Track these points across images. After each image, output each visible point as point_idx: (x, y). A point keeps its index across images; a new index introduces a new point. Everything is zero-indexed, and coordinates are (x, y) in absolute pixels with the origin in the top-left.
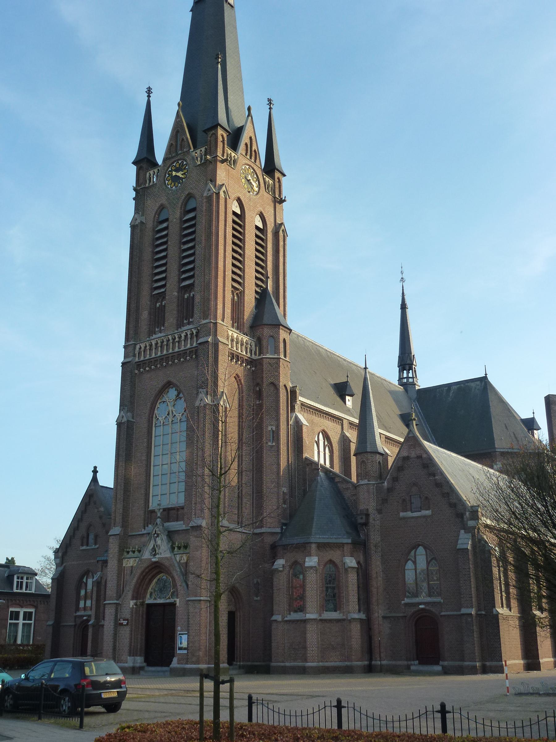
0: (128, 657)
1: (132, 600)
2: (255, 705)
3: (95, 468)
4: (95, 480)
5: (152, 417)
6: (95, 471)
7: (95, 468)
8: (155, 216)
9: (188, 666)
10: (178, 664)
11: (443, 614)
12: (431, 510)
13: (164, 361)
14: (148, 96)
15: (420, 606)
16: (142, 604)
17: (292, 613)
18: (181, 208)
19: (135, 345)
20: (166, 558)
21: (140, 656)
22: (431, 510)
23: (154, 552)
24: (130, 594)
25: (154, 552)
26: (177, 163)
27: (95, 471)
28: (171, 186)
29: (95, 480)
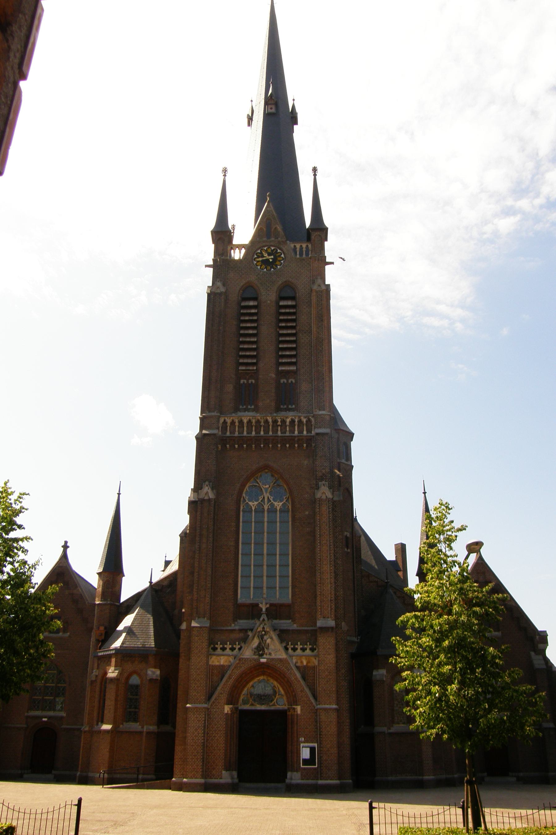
0: (224, 772)
1: (228, 704)
2: (525, 819)
3: (66, 542)
4: (64, 556)
5: (240, 501)
6: (66, 547)
7: (66, 542)
8: (239, 291)
9: (320, 782)
10: (302, 779)
11: (64, 726)
12: (500, 632)
13: (262, 442)
14: (314, 175)
15: (44, 719)
16: (237, 708)
17: (124, 723)
18: (276, 292)
19: (219, 417)
20: (281, 660)
21: (235, 770)
22: (500, 632)
23: (260, 650)
24: (224, 697)
25: (260, 650)
26: (268, 248)
27: (66, 547)
28: (262, 268)
29: (64, 556)
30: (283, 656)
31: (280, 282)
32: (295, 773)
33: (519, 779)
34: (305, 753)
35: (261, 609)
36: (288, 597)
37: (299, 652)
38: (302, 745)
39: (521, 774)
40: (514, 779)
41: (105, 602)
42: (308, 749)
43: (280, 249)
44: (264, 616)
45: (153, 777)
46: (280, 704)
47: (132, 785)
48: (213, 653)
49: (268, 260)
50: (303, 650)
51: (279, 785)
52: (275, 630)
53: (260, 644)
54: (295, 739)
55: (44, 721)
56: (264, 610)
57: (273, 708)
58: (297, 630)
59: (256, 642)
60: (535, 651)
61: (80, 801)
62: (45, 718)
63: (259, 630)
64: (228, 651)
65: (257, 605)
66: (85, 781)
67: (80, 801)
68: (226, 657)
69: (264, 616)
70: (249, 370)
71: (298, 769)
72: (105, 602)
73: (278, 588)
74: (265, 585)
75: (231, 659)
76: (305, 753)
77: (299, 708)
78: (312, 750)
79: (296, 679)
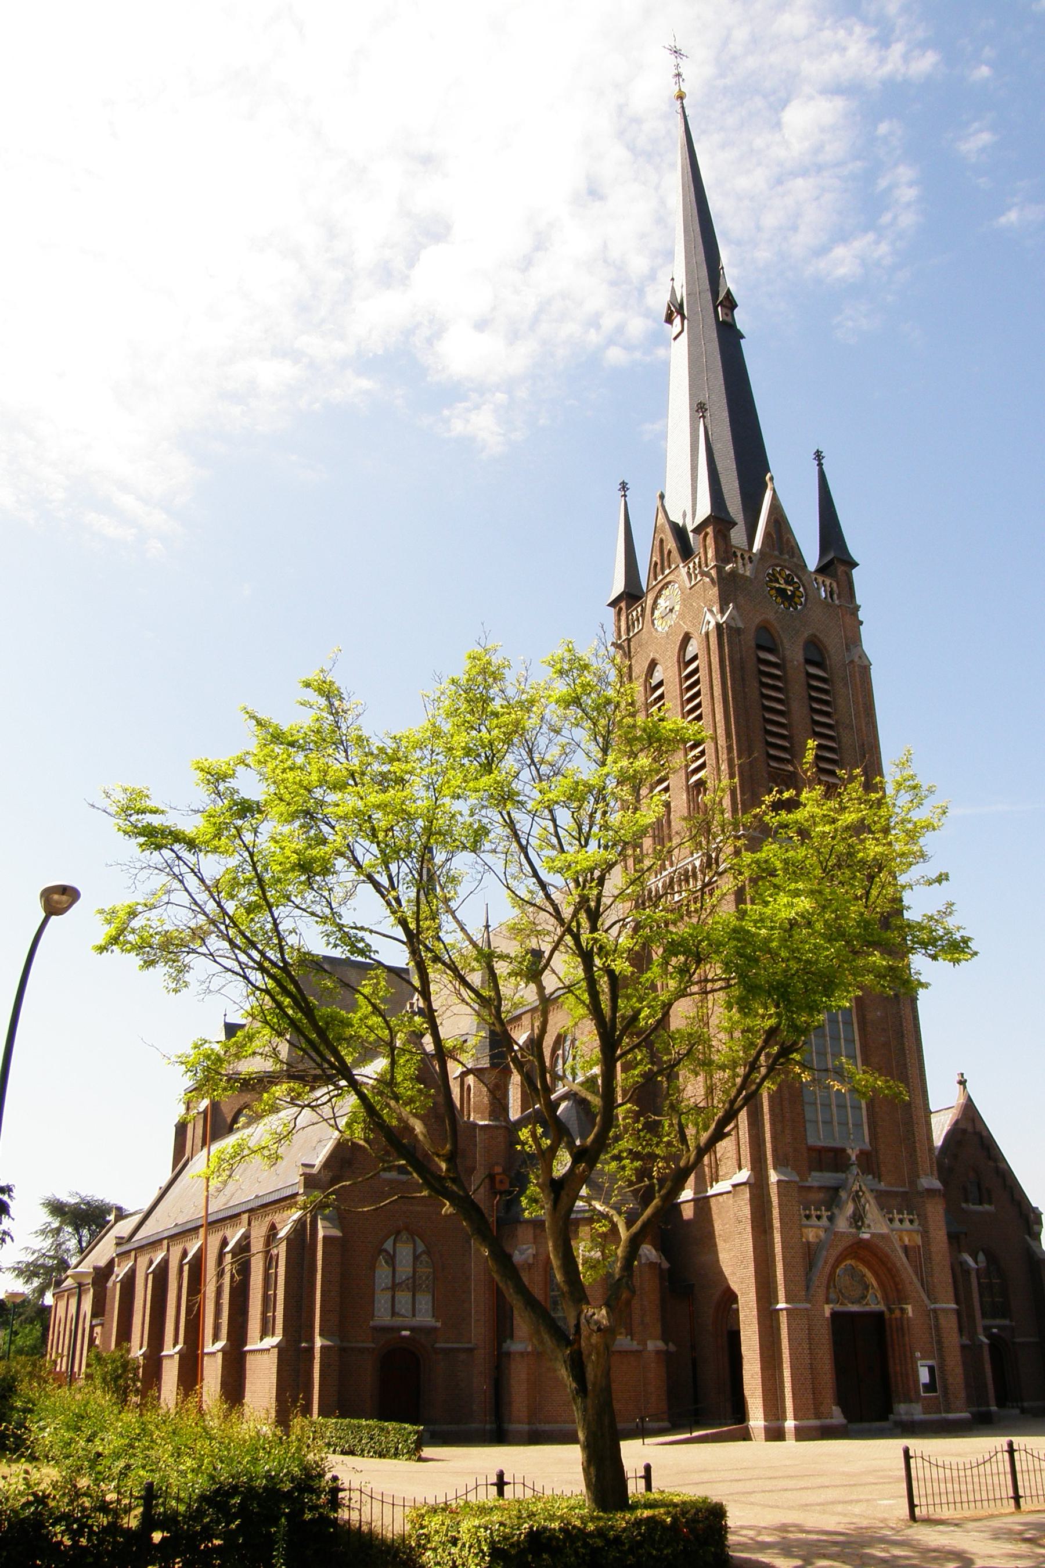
25: (858, 1219)
30: (885, 1230)
31: (806, 635)
32: (914, 1405)
33: (1023, 1411)
34: (924, 1376)
35: (849, 1157)
36: (864, 1141)
37: (897, 1224)
38: (919, 1363)
39: (1026, 1404)
40: (1017, 1411)
41: (497, 1123)
42: (926, 1369)
43: (798, 578)
44: (855, 1170)
45: (666, 1424)
46: (875, 1304)
47: (707, 1435)
48: (808, 1223)
49: (785, 590)
50: (901, 1221)
51: (884, 1424)
52: (872, 1191)
53: (856, 1209)
54: (909, 1354)
55: (405, 1337)
56: (854, 1158)
57: (867, 1309)
58: (886, 1191)
59: (850, 1209)
60: (1030, 1235)
61: (648, 1468)
62: (405, 1330)
63: (854, 1189)
64: (814, 1221)
65: (844, 1150)
66: (499, 1437)
67: (648, 1468)
68: (815, 1230)
69: (855, 1170)
70: (784, 770)
71: (918, 1399)
72: (497, 1123)
73: (851, 1126)
74: (835, 1118)
75: (822, 1234)
76: (924, 1376)
77: (909, 1308)
78: (931, 1369)
79: (903, 1265)
